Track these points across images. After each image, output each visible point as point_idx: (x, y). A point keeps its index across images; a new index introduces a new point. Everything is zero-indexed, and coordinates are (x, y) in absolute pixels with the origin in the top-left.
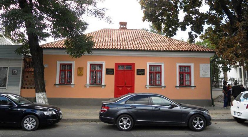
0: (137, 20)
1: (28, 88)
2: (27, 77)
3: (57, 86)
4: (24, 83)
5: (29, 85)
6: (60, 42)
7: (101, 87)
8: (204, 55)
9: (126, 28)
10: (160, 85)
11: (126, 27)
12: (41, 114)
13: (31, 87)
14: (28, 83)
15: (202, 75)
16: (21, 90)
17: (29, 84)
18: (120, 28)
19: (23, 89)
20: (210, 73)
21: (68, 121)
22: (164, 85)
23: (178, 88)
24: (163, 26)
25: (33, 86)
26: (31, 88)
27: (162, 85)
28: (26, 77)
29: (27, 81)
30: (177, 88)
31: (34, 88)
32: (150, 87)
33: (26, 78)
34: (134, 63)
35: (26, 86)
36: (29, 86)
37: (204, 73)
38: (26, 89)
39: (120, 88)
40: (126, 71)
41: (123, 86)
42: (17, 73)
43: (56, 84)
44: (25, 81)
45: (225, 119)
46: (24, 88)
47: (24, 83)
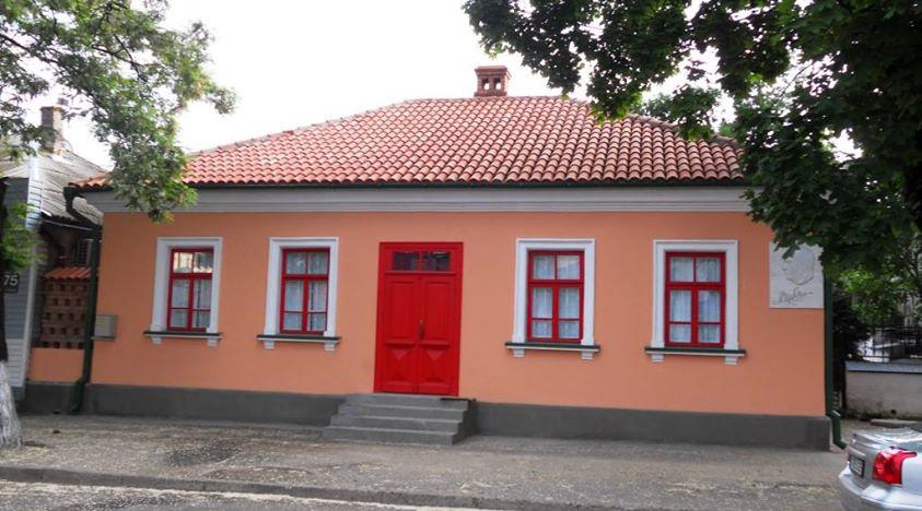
0: (440, 55)
1: (57, 345)
2: (56, 302)
3: (157, 340)
4: (47, 325)
5: (63, 336)
6: (435, 163)
7: (323, 344)
8: (287, 201)
9: (502, 93)
10: (576, 342)
11: (503, 88)
12: (889, 483)
13: (70, 340)
14: (57, 326)
15: (783, 294)
16: (31, 352)
17: (64, 331)
18: (476, 95)
19: (40, 351)
20: (821, 286)
21: (44, 476)
22: (591, 344)
23: (658, 358)
24: (587, 69)
25: (75, 340)
26: (69, 346)
27: (727, 347)
28: (52, 302)
29: (54, 317)
30: (654, 357)
31: (80, 344)
32: (525, 350)
33: (51, 308)
34: (461, 244)
35: (52, 339)
36: (62, 339)
37: (789, 289)
38: (51, 351)
39: (400, 354)
40: (425, 279)
41: (410, 342)
42: (16, 287)
43: (152, 330)
44: (83, 317)
45: (146, 476)
46: (46, 345)
47: (47, 325)
